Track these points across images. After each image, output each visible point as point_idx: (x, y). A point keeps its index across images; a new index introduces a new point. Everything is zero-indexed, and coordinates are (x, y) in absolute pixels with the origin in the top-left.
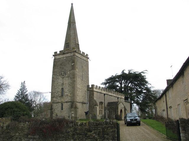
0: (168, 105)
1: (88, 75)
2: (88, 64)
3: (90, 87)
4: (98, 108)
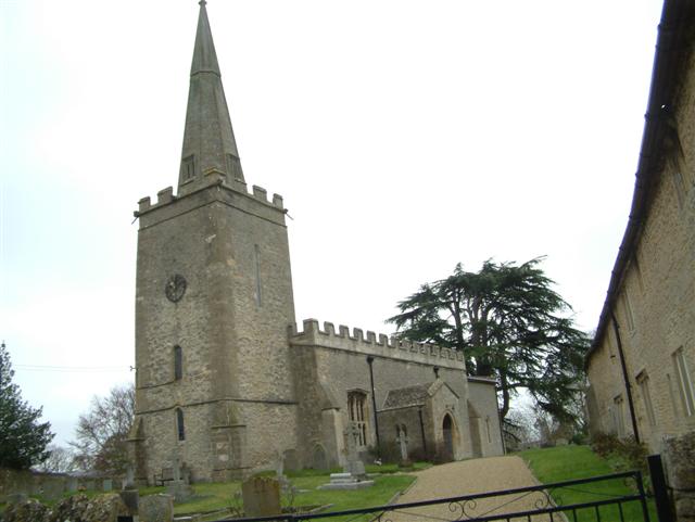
0: (629, 367)
1: (290, 280)
2: (286, 234)
3: (300, 329)
4: (339, 419)
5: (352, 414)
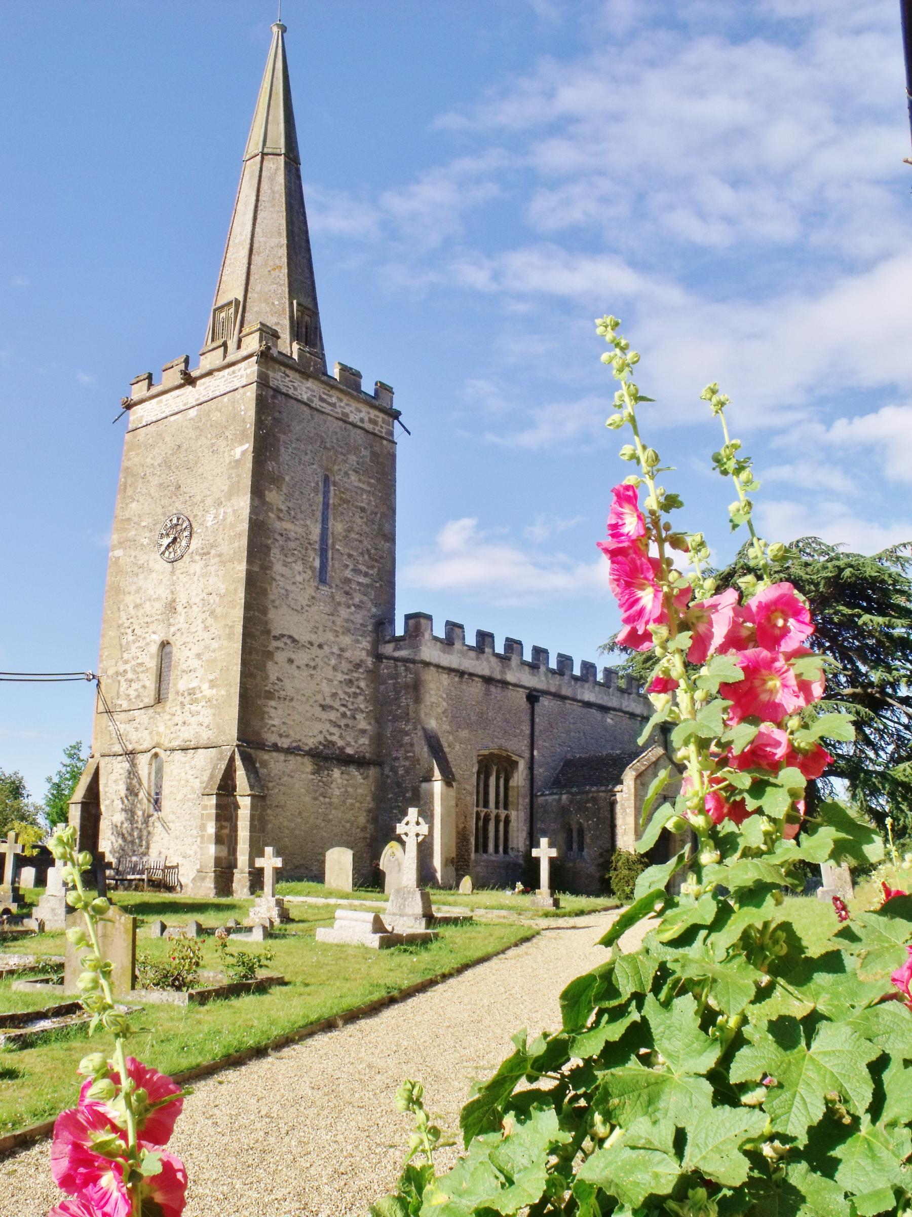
2: (393, 457)
5: (486, 794)
